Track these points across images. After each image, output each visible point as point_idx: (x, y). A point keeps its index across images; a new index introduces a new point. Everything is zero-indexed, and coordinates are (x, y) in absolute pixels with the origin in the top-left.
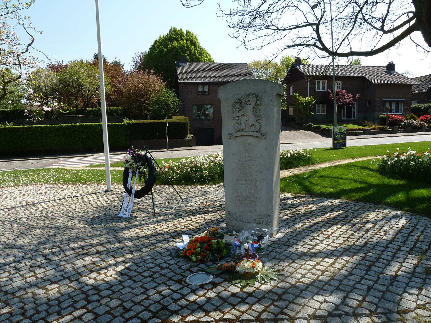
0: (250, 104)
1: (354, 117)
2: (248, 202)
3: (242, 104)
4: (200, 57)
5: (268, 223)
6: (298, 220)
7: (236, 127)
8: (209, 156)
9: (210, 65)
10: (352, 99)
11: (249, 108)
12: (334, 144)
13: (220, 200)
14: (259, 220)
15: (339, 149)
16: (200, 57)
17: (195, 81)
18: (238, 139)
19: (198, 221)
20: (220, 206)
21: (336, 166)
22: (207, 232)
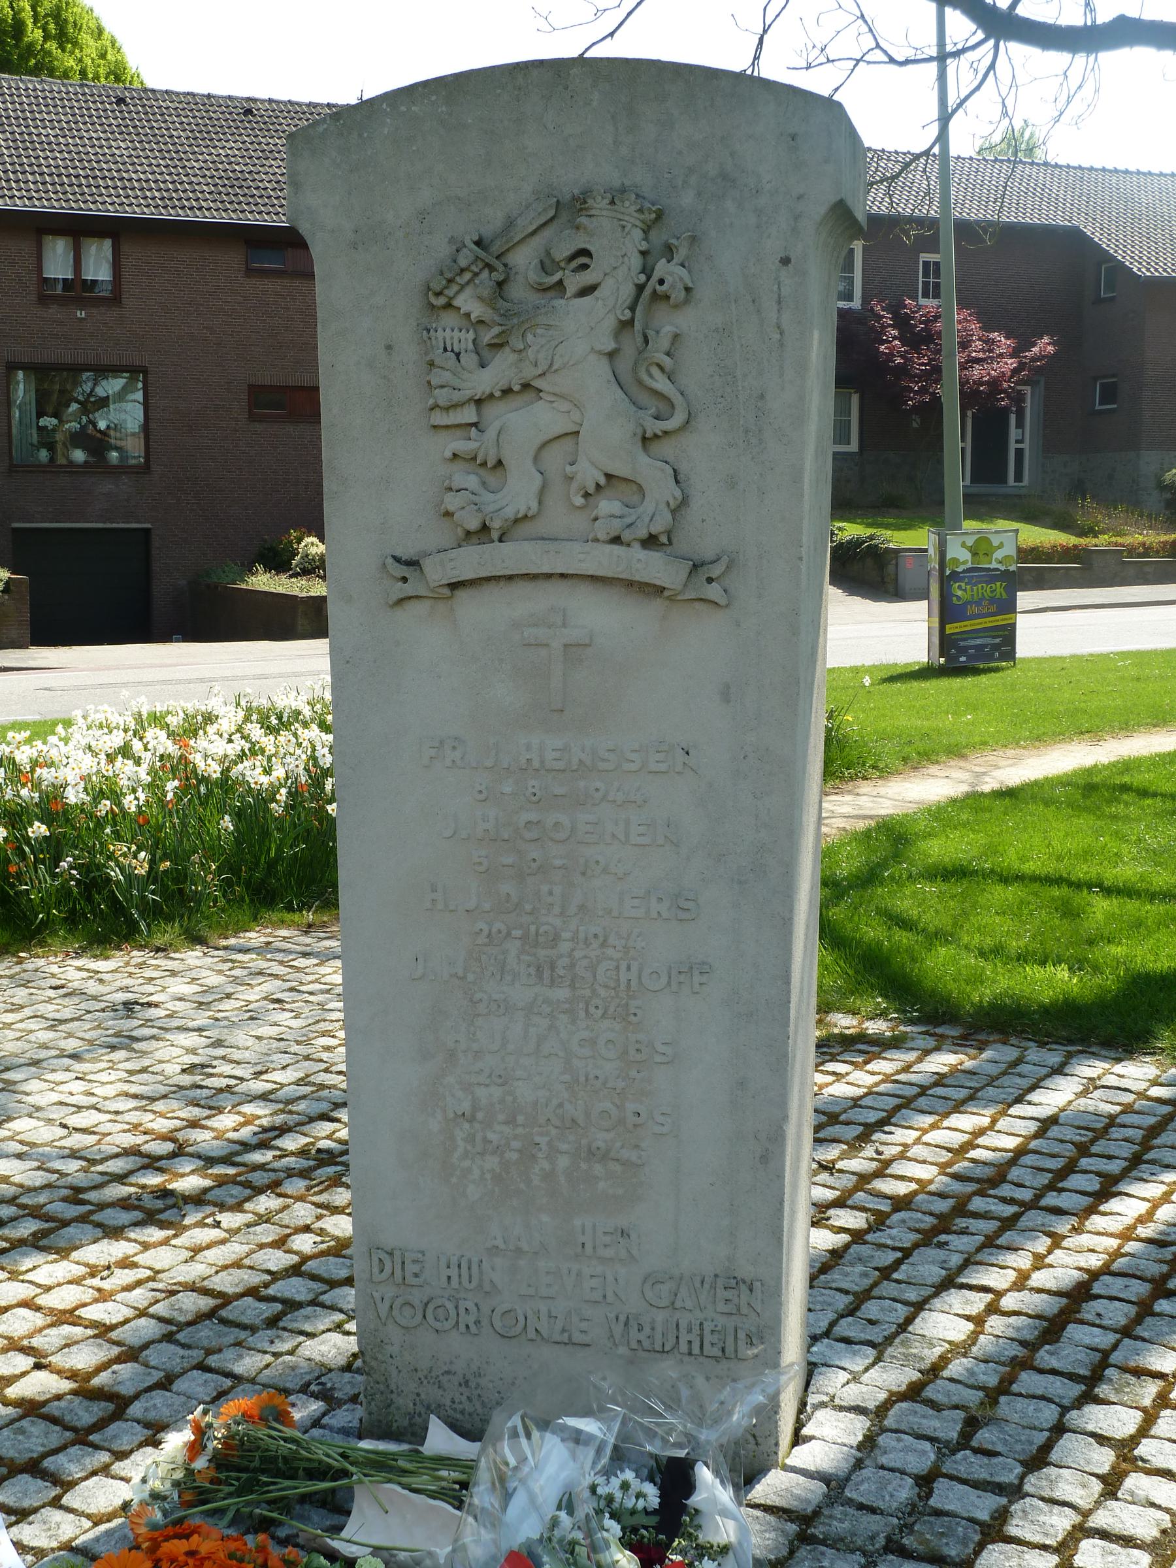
0: (587, 291)
1: (1019, 477)
2: (563, 1162)
3: (518, 291)
4: (52, 46)
5: (730, 1331)
6: (927, 1266)
7: (452, 502)
8: (139, 718)
9: (121, 101)
10: (1012, 363)
11: (581, 329)
12: (946, 643)
13: (259, 1086)
14: (660, 1317)
15: (976, 672)
16: (52, 46)
17: (20, 205)
18: (471, 609)
19: (95, 1312)
20: (264, 1145)
21: (1009, 794)
22: (195, 1448)
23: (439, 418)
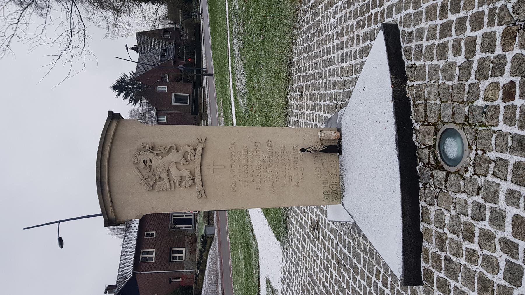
0: (151, 161)
7: (187, 185)
11: (157, 162)
23: (173, 188)
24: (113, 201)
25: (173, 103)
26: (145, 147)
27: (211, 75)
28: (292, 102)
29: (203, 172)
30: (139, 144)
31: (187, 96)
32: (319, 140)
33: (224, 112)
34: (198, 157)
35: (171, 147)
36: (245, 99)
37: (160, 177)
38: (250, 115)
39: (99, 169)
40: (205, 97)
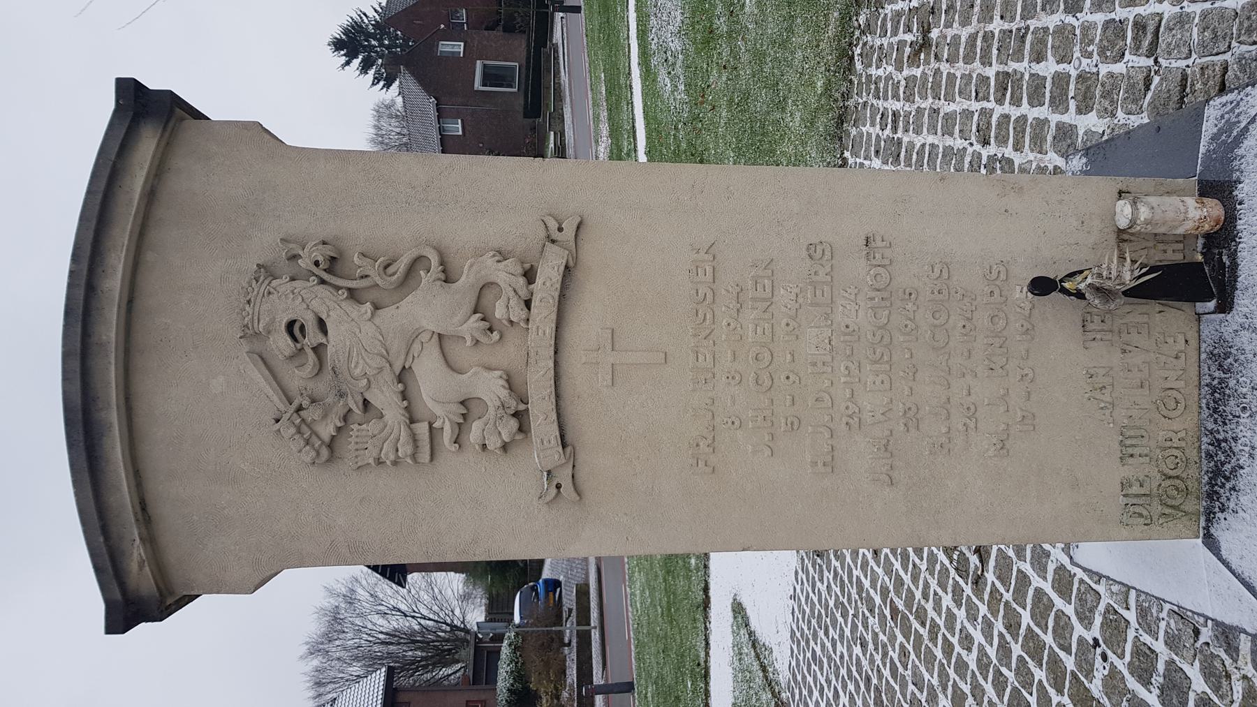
0: (322, 325)
7: (494, 443)
11: (352, 332)
23: (425, 455)
24: (150, 510)
25: (477, 85)
26: (294, 257)
27: (577, 9)
28: (873, 71)
29: (565, 382)
30: (264, 244)
31: (513, 68)
32: (1112, 238)
33: (610, 110)
34: (544, 312)
35: (417, 262)
36: (679, 70)
37: (366, 403)
38: (696, 118)
39: (76, 364)
40: (559, 72)
